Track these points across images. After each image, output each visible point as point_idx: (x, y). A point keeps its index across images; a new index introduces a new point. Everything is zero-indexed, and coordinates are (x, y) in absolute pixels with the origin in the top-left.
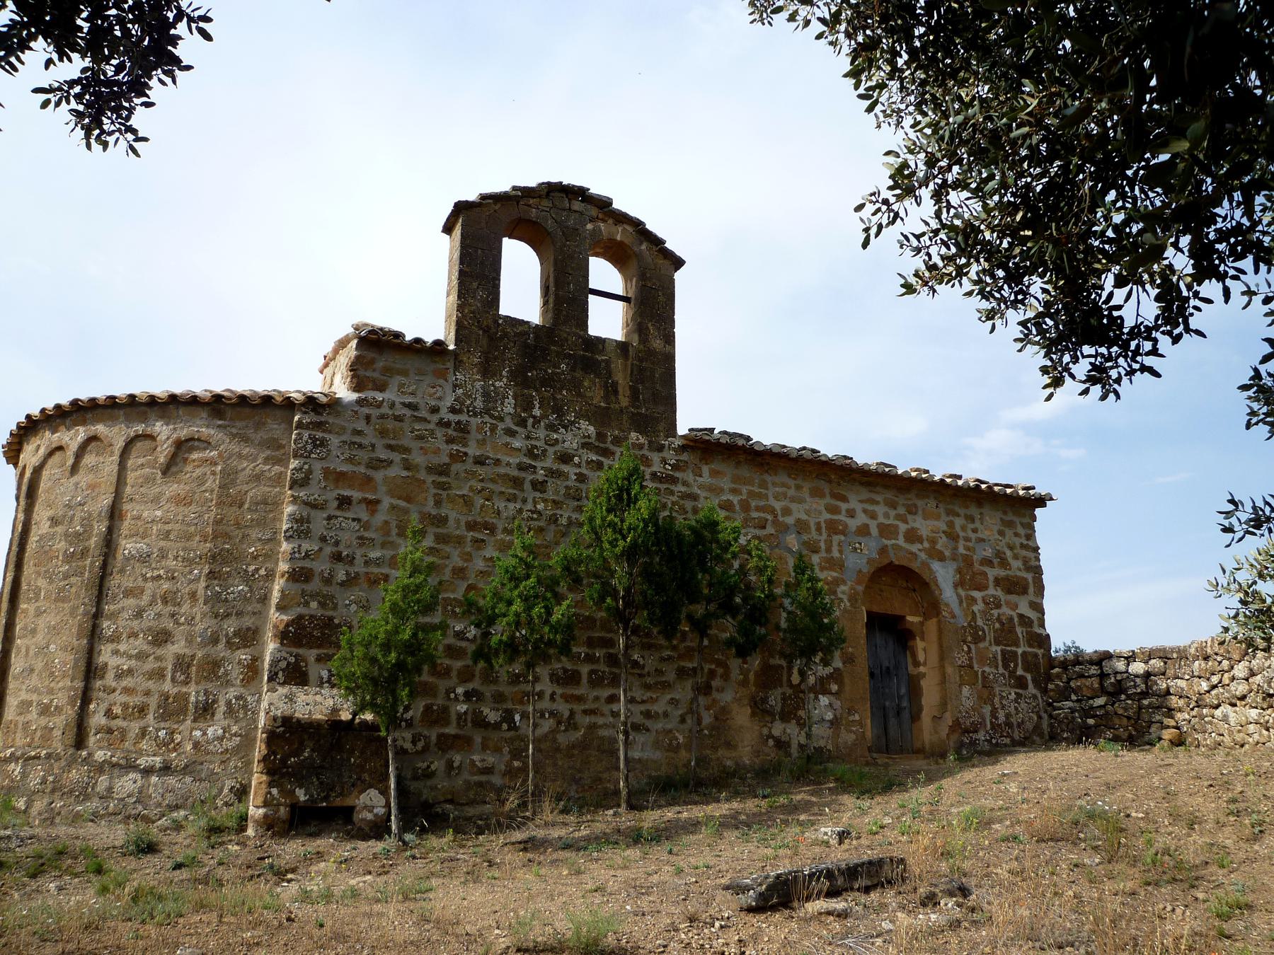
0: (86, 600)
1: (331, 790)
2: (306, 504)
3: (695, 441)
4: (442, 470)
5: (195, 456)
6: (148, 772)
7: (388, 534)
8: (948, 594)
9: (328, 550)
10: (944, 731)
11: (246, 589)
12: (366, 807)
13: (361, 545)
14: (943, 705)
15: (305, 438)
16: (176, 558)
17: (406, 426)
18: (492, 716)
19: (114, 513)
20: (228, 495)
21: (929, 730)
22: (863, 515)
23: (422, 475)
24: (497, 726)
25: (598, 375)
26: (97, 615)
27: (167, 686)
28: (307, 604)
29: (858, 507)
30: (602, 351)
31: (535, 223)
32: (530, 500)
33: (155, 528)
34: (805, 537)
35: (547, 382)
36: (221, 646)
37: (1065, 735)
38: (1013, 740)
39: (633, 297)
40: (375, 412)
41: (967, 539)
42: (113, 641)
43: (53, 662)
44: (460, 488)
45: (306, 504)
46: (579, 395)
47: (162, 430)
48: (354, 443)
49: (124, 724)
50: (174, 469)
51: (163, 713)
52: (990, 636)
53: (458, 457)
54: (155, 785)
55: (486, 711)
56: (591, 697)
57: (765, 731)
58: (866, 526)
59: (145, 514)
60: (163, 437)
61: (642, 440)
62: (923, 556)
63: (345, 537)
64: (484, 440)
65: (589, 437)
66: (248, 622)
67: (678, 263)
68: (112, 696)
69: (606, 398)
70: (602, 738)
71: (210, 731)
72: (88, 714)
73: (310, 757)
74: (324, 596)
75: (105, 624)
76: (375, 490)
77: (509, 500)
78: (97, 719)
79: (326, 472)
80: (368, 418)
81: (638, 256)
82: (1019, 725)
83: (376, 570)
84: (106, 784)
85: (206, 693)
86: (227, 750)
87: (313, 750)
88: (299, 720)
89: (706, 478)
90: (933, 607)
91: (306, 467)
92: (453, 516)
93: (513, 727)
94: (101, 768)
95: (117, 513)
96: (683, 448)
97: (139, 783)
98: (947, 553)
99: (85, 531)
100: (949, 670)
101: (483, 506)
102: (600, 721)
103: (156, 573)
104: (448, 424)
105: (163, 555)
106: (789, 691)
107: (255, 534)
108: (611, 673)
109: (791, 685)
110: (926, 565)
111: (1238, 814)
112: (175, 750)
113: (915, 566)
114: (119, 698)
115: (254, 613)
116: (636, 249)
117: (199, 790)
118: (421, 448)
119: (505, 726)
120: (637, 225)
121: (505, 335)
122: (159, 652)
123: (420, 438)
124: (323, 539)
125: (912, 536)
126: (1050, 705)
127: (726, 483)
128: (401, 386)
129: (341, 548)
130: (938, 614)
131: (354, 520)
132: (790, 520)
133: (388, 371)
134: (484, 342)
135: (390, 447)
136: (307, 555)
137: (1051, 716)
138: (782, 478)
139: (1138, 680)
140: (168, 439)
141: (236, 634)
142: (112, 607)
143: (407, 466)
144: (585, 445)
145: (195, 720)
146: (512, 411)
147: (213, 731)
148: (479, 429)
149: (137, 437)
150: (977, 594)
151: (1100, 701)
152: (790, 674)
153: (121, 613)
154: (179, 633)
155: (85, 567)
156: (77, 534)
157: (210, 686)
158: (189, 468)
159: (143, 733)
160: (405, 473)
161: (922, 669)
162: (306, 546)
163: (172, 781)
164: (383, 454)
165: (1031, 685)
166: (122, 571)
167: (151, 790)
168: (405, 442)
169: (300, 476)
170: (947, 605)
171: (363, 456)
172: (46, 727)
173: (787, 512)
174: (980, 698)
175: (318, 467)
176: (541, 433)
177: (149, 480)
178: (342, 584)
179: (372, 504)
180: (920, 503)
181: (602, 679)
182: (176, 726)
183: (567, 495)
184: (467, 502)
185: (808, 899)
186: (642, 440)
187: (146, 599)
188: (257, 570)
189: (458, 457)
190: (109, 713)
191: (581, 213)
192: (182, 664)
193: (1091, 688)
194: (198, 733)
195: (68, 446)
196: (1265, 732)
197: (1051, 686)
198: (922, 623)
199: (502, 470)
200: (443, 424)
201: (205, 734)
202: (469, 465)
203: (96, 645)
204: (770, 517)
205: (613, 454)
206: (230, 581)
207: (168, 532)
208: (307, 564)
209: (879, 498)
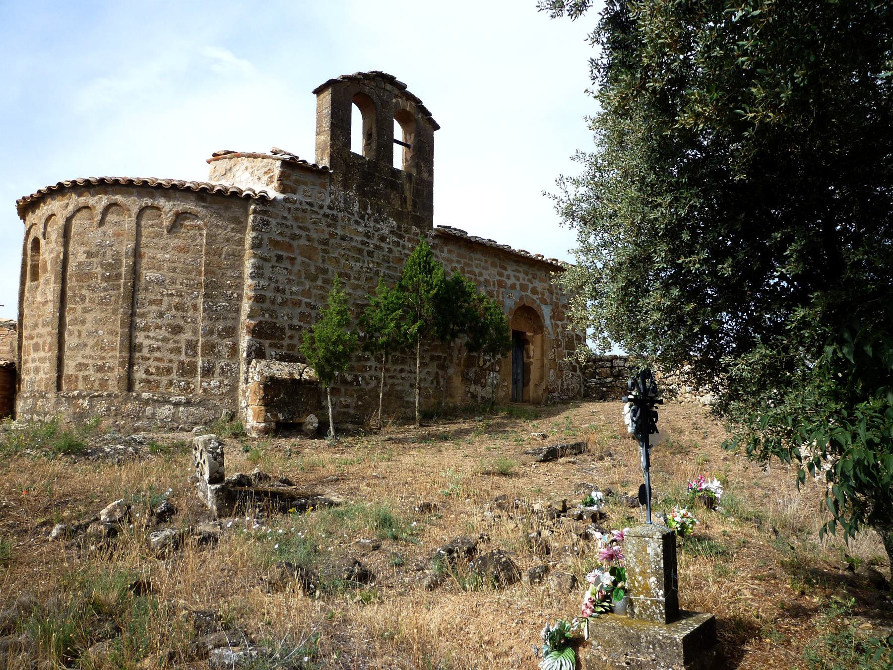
0: (124, 305)
1: (294, 414)
2: (261, 258)
3: (443, 233)
4: (325, 242)
5: (188, 223)
6: (177, 404)
7: (300, 277)
8: (547, 322)
9: (273, 285)
10: (541, 392)
11: (227, 304)
12: (309, 423)
13: (289, 283)
14: (541, 378)
15: (259, 219)
16: (182, 284)
17: (307, 215)
18: (349, 378)
19: (137, 254)
20: (212, 249)
21: (532, 391)
22: (513, 278)
23: (316, 245)
24: (351, 383)
25: (398, 192)
26: (133, 314)
27: (183, 357)
28: (263, 315)
29: (512, 274)
30: (399, 178)
31: (368, 96)
32: (366, 262)
33: (165, 265)
34: (488, 289)
35: (375, 194)
36: (215, 336)
38: (569, 397)
39: (412, 145)
40: (293, 207)
41: (557, 294)
42: (145, 330)
43: (102, 341)
44: (333, 253)
45: (261, 258)
46: (389, 203)
47: (167, 206)
48: (283, 224)
49: (158, 378)
50: (175, 230)
52: (563, 345)
53: (333, 235)
54: (183, 412)
55: (346, 375)
56: (393, 369)
57: (467, 389)
58: (515, 284)
60: (167, 209)
61: (418, 231)
62: (538, 301)
63: (281, 278)
64: (345, 226)
65: (393, 227)
66: (230, 323)
67: (437, 127)
69: (401, 205)
70: (397, 391)
71: (212, 383)
72: (133, 372)
73: (284, 397)
74: (271, 311)
75: (138, 320)
76: (293, 252)
77: (356, 261)
78: (139, 374)
79: (270, 239)
80: (289, 209)
81: (416, 121)
82: (572, 390)
83: (295, 298)
84: (151, 411)
85: (208, 362)
87: (284, 394)
88: (277, 378)
89: (445, 254)
90: (539, 328)
91: (260, 236)
92: (331, 268)
93: (358, 384)
95: (138, 254)
96: (436, 236)
97: (172, 411)
98: (548, 301)
99: (115, 263)
100: (546, 361)
101: (345, 264)
102: (396, 382)
103: (170, 292)
104: (328, 216)
105: (173, 281)
106: (478, 369)
107: (230, 273)
108: (402, 357)
109: (479, 366)
110: (539, 307)
111: (697, 429)
112: (191, 393)
113: (535, 307)
114: (152, 363)
115: (233, 319)
116: (416, 117)
117: (209, 414)
118: (315, 229)
119: (355, 383)
120: (418, 102)
121: (354, 164)
122: (176, 338)
123: (315, 223)
124: (270, 279)
125: (534, 291)
126: (586, 380)
127: (454, 257)
128: (304, 191)
129: (279, 284)
130: (542, 332)
131: (284, 268)
132: (482, 279)
133: (297, 182)
134: (344, 168)
135: (299, 227)
136: (263, 288)
137: (585, 386)
138: (479, 256)
140: (170, 211)
141: (223, 330)
142: (142, 311)
143: (309, 239)
144: (392, 232)
145: (203, 377)
146: (358, 210)
147: (214, 383)
148: (343, 220)
149: (147, 207)
150: (559, 323)
151: (610, 380)
152: (479, 361)
153: (148, 315)
154: (188, 328)
155: (120, 285)
156: (110, 264)
157: (210, 358)
158: (183, 230)
159: (171, 383)
160: (308, 243)
161: (531, 360)
162: (262, 283)
163: (192, 409)
164: (297, 232)
165: (578, 370)
166: (146, 289)
168: (308, 224)
169: (257, 241)
170: (547, 328)
171: (288, 231)
172: (102, 379)
173: (481, 274)
174: (557, 376)
175: (266, 237)
176: (371, 224)
177: (159, 235)
178: (280, 305)
179: (292, 260)
180: (538, 273)
181: (397, 360)
182: (190, 380)
183: (383, 260)
184: (337, 261)
185: (561, 457)
186: (418, 231)
187: (164, 307)
188: (232, 294)
189: (333, 235)
190: (147, 371)
191: (390, 92)
192: (191, 346)
193: (606, 373)
195: (94, 207)
196: (694, 397)
197: (587, 371)
198: (533, 336)
199: (354, 244)
200: (326, 216)
201: (209, 384)
202: (338, 240)
203: (133, 332)
204: (473, 277)
205: (404, 238)
206: (217, 299)
207: (175, 268)
208: (263, 293)
209: (521, 269)
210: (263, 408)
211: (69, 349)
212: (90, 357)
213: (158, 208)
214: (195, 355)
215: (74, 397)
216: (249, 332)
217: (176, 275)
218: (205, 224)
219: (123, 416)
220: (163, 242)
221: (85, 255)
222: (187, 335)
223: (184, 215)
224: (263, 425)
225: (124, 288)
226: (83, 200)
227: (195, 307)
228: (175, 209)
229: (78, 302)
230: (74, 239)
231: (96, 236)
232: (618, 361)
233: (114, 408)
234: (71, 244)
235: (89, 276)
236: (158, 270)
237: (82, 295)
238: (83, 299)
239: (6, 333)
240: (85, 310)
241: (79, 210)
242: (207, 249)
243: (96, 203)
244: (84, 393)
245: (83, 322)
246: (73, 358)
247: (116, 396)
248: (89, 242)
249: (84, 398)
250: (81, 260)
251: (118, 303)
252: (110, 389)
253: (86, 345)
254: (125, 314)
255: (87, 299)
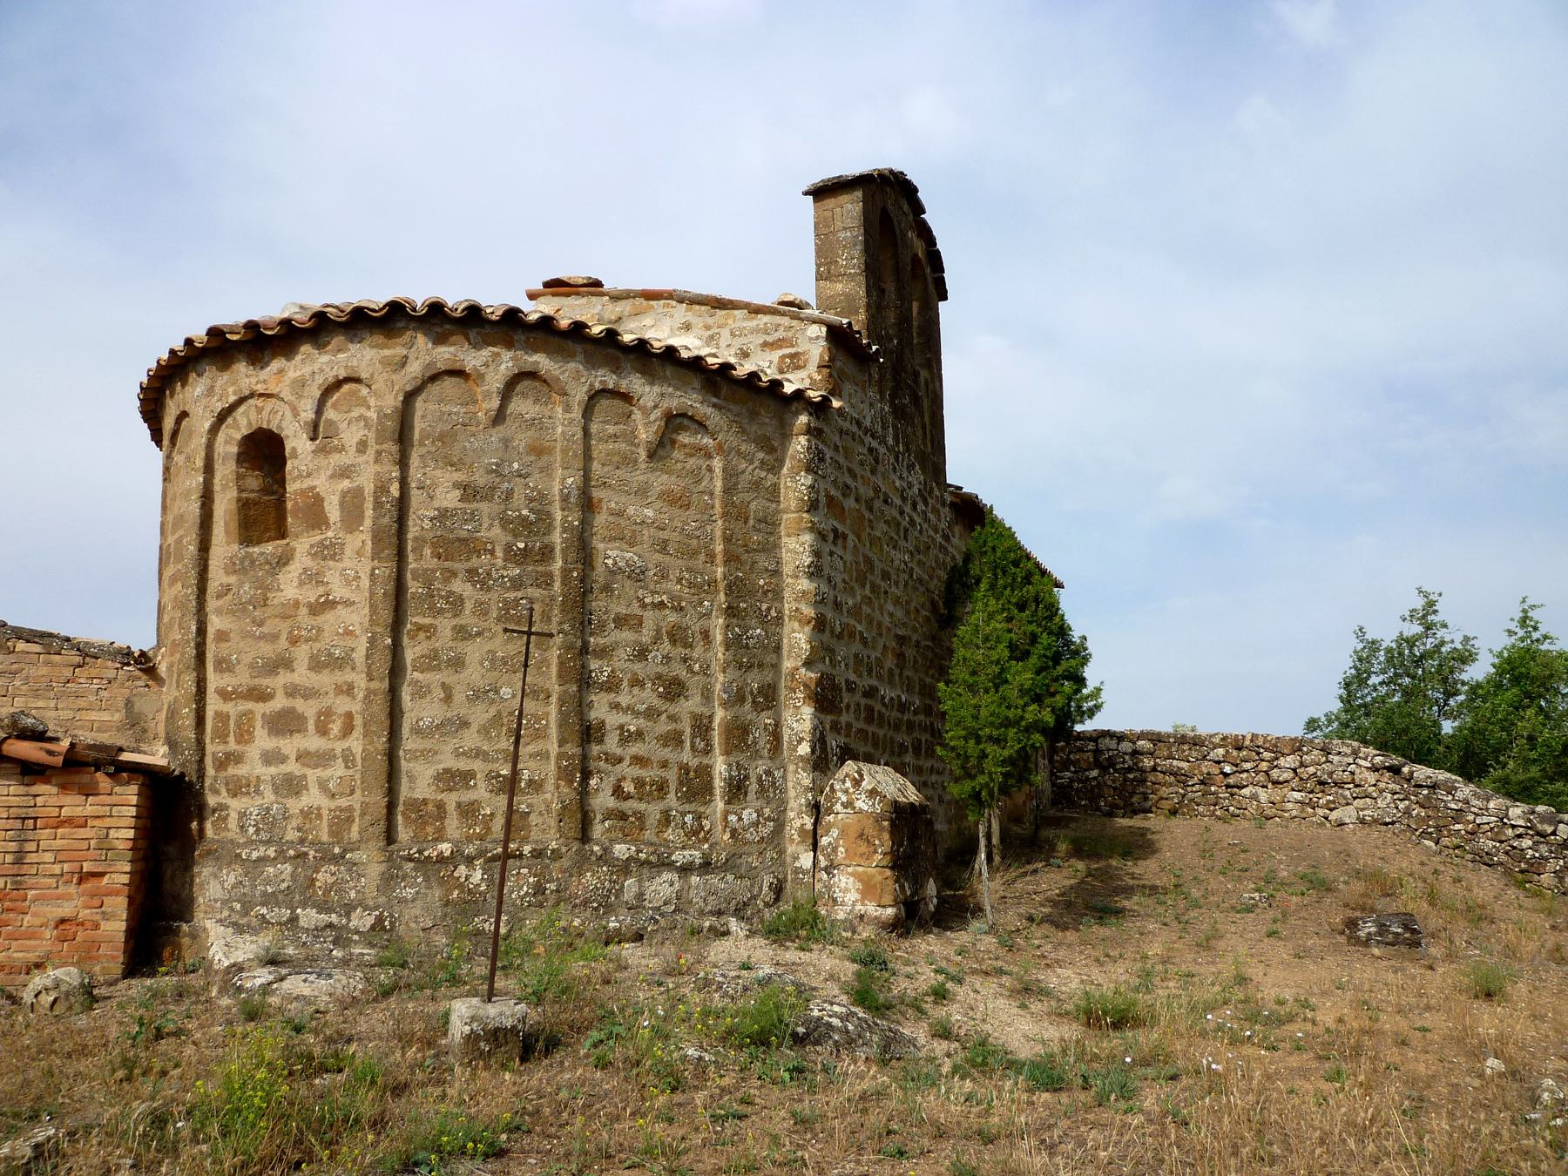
0: (566, 627)
6: (686, 870)
16: (679, 581)
27: (686, 756)
36: (748, 706)
37: (1083, 803)
42: (609, 690)
49: (642, 806)
50: (661, 452)
51: (687, 792)
59: (631, 510)
67: (945, 298)
68: (618, 768)
75: (594, 664)
78: (603, 800)
84: (635, 889)
86: (763, 838)
94: (625, 868)
97: (677, 886)
99: (539, 520)
103: (657, 599)
112: (706, 840)
114: (628, 770)
122: (673, 709)
139: (1127, 757)
140: (656, 407)
145: (728, 802)
147: (749, 815)
149: (604, 392)
151: (1095, 773)
155: (551, 575)
157: (741, 757)
158: (676, 454)
159: (666, 819)
163: (714, 880)
166: (607, 588)
167: (692, 893)
177: (628, 461)
182: (702, 809)
187: (646, 636)
188: (769, 609)
190: (618, 791)
193: (1087, 761)
194: (733, 818)
195: (481, 376)
201: (740, 819)
210: (888, 872)
211: (417, 731)
212: (478, 754)
213: (626, 398)
214: (708, 751)
215: (441, 859)
216: (810, 698)
217: (668, 558)
218: (720, 448)
219: (575, 906)
220: (639, 477)
221: (458, 493)
222: (690, 705)
223: (678, 420)
224: (890, 911)
225: (563, 584)
226: (445, 354)
227: (706, 635)
228: (665, 404)
229: (441, 611)
230: (423, 450)
231: (485, 447)
232: (1107, 740)
233: (553, 886)
234: (414, 461)
235: (470, 546)
236: (632, 545)
237: (451, 593)
238: (457, 603)
239: (111, 674)
240: (462, 633)
241: (434, 378)
242: (725, 505)
243: (486, 365)
244: (470, 850)
245: (457, 663)
246: (427, 755)
247: (557, 856)
248: (467, 460)
249: (469, 861)
250: (445, 504)
251: (549, 620)
252: (534, 835)
253: (465, 724)
254: (568, 647)
255: (469, 605)
